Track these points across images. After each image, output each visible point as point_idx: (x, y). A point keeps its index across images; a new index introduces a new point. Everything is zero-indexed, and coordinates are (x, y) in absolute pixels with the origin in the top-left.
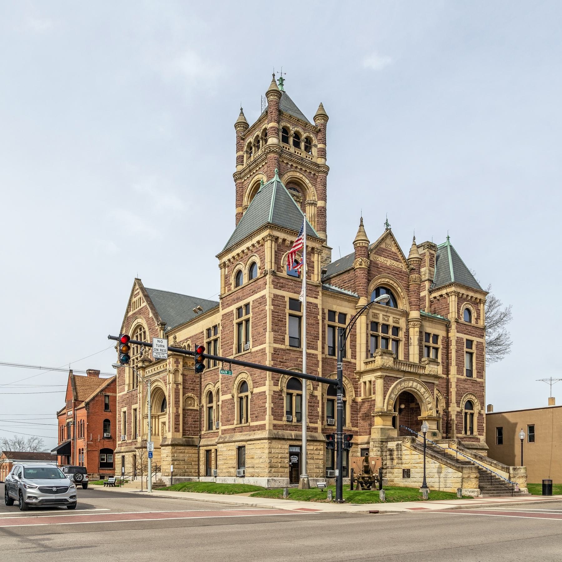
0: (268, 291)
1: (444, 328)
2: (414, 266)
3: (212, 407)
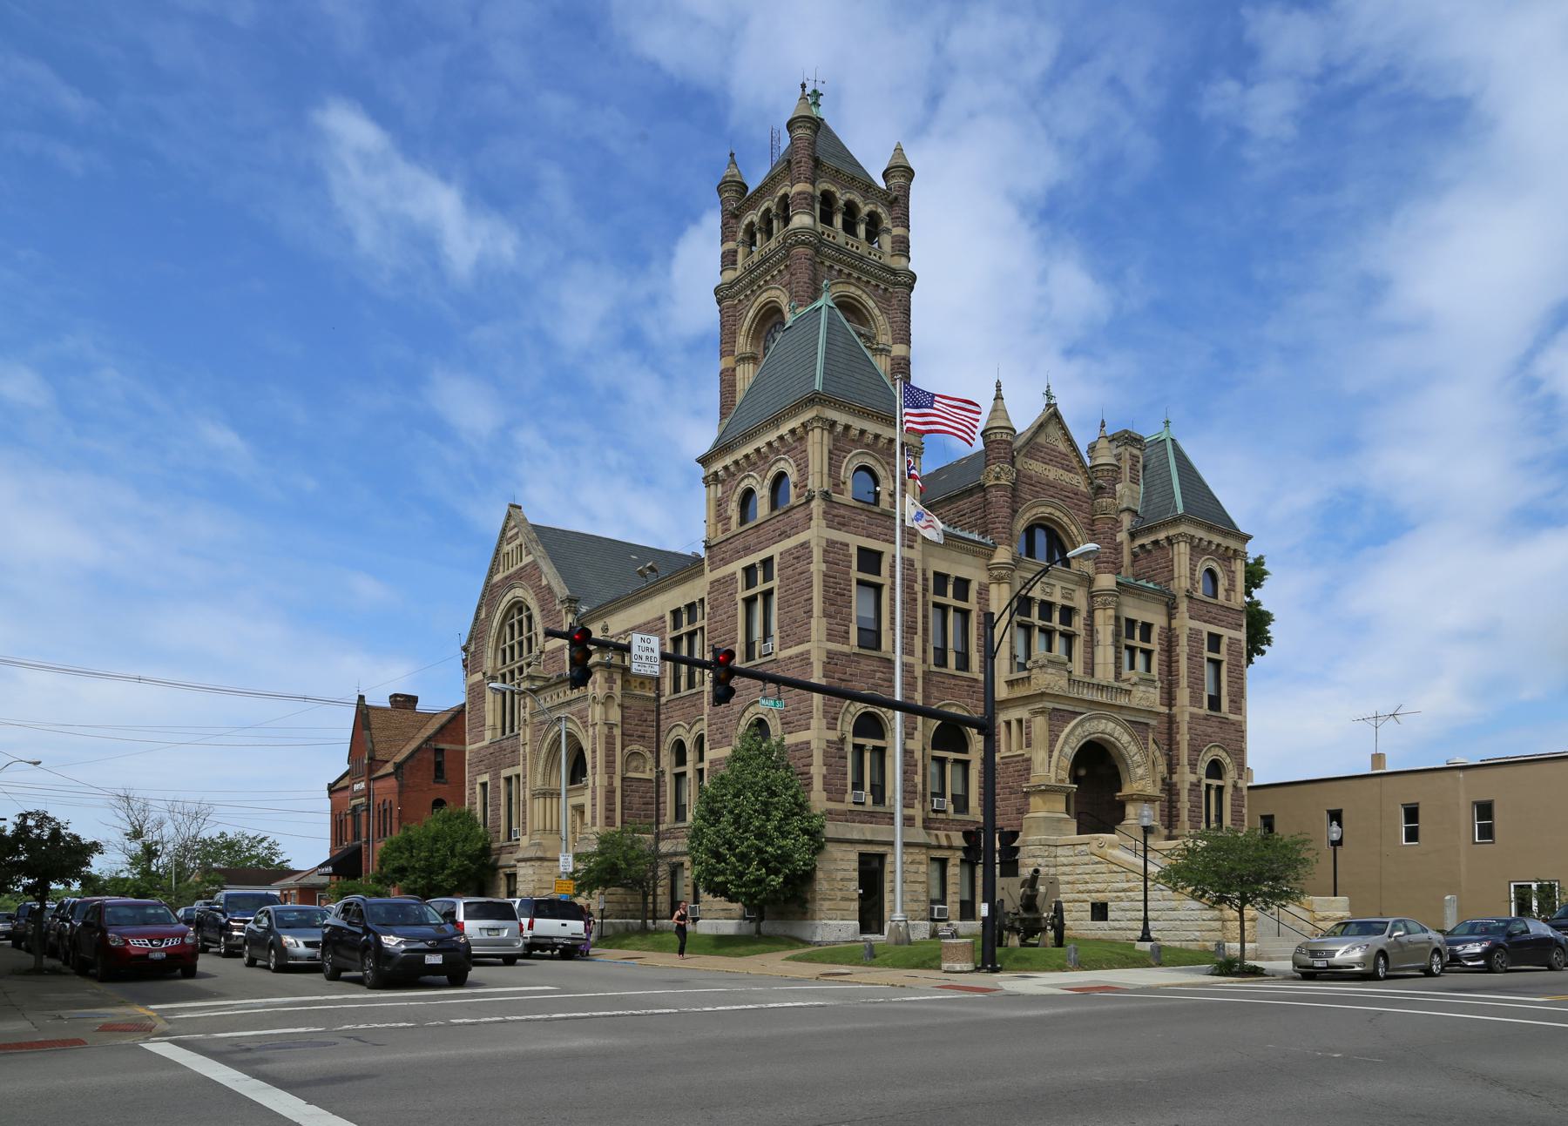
0: (816, 533)
1: (1163, 609)
2: (1100, 483)
3: (684, 774)
